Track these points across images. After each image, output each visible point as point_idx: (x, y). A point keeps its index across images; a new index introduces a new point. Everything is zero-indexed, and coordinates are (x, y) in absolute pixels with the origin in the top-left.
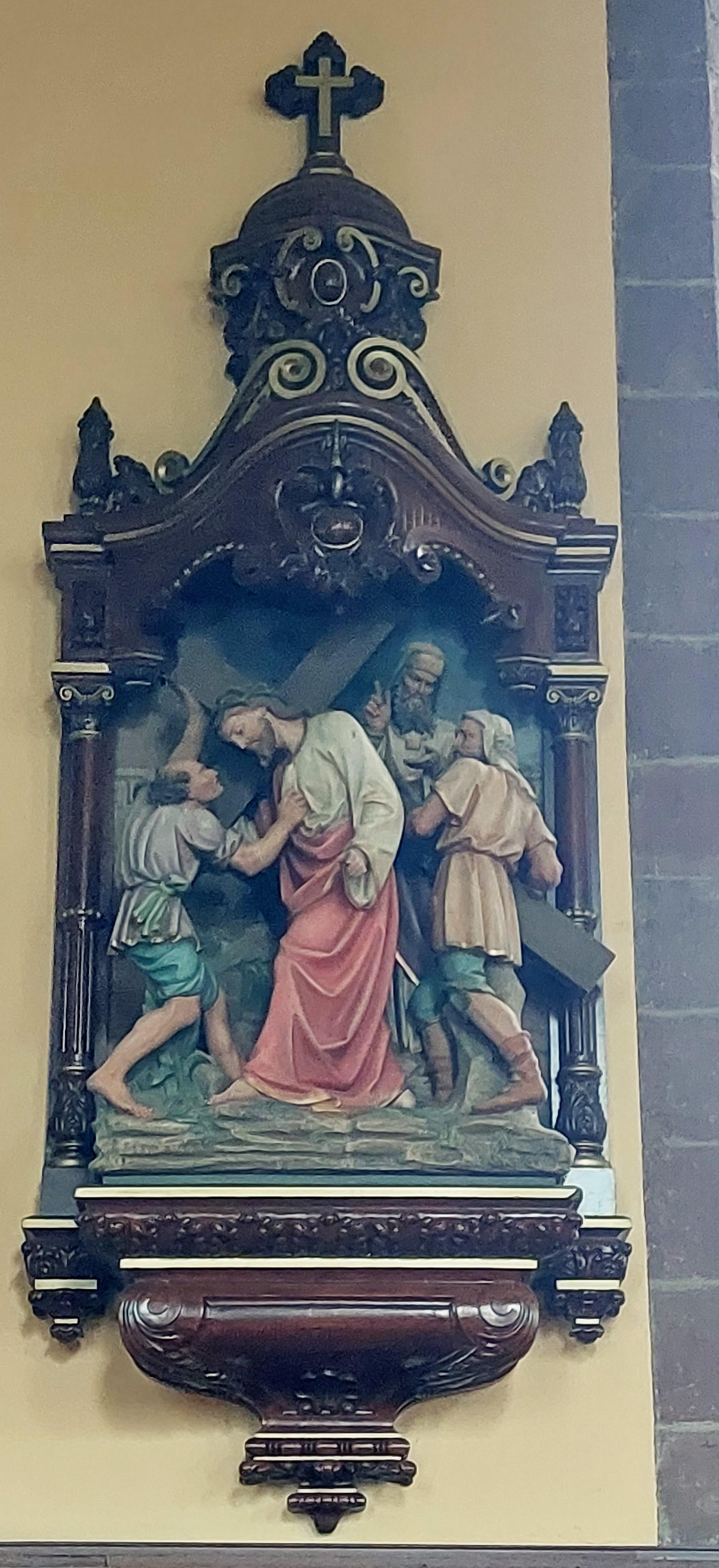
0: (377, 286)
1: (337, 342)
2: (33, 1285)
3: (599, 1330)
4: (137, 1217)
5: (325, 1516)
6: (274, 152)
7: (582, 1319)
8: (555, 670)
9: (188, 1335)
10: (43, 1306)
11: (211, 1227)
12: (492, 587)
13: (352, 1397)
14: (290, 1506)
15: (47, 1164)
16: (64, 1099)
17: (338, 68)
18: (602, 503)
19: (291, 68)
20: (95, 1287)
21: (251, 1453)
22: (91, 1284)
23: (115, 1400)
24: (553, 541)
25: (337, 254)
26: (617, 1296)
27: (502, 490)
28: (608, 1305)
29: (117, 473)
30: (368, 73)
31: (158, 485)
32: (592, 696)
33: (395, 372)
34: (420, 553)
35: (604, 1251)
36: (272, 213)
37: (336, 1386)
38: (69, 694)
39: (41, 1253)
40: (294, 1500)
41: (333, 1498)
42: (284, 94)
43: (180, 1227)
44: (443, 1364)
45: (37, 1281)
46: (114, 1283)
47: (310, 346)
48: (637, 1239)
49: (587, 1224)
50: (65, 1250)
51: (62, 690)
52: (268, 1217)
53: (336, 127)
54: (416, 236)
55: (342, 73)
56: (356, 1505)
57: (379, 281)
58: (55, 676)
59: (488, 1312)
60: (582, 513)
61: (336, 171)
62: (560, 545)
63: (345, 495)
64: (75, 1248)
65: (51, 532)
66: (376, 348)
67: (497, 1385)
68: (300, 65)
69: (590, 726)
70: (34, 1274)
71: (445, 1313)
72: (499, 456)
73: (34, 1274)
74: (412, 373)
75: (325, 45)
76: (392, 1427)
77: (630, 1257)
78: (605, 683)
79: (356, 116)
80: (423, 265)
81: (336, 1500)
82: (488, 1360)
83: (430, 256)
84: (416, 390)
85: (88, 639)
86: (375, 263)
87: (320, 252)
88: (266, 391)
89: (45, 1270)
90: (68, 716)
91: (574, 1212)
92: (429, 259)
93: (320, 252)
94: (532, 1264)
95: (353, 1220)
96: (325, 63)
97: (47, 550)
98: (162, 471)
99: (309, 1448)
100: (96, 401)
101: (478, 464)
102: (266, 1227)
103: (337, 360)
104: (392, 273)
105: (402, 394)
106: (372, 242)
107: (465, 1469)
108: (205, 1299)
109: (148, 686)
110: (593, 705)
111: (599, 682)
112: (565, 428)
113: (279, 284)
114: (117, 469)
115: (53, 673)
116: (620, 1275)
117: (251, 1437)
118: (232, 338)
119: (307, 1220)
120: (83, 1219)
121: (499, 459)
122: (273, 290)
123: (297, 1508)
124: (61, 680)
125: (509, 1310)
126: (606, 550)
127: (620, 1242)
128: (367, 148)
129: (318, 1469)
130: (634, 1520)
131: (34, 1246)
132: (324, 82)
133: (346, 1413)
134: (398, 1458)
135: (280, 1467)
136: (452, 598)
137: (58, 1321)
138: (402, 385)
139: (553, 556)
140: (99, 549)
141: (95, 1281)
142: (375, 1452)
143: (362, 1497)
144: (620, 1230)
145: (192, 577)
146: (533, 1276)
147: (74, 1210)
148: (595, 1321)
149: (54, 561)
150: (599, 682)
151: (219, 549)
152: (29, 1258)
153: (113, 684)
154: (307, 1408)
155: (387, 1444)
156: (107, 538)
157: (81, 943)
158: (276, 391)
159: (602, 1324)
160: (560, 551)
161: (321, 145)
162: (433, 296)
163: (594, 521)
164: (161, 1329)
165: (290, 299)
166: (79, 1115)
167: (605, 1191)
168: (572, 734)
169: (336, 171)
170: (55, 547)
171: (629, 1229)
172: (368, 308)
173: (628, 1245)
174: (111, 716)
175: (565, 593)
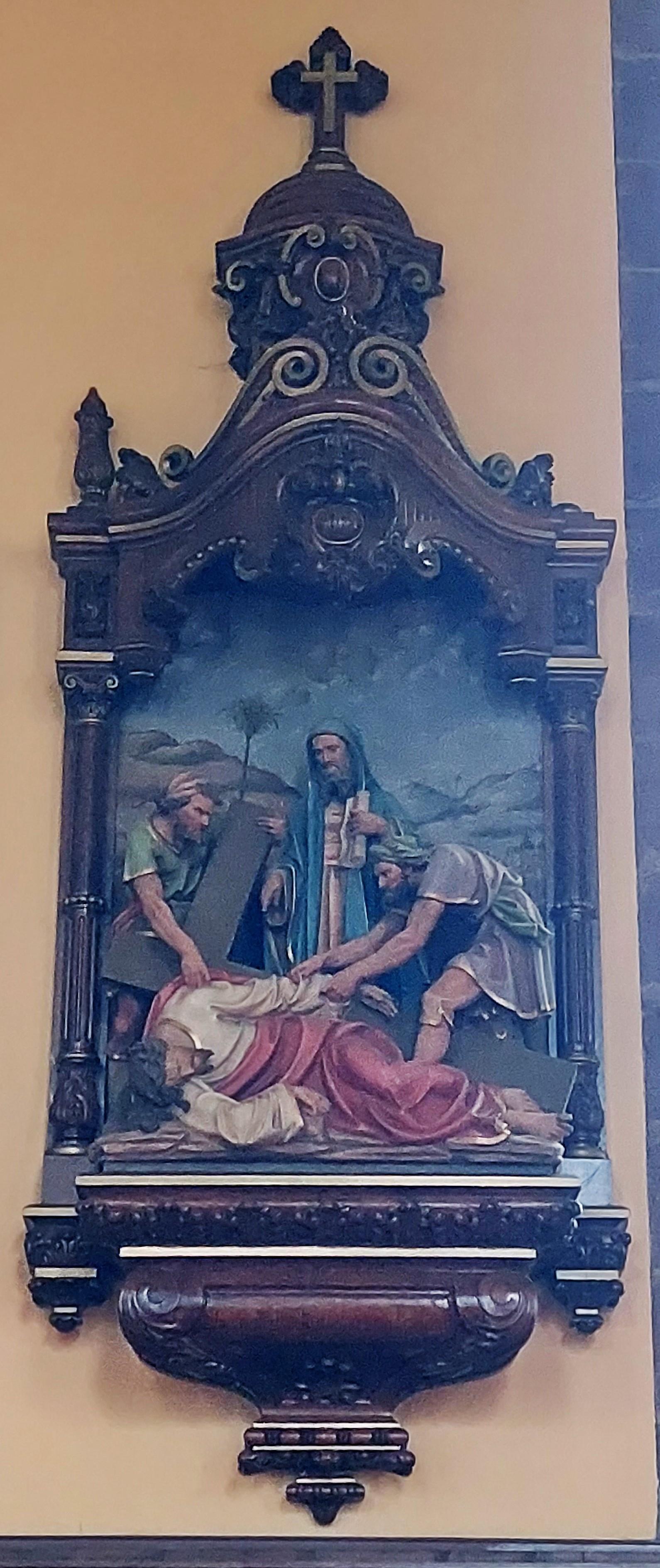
1: (340, 341)
2: (32, 1272)
3: (75, 1318)
5: (324, 1507)
6: (282, 147)
7: (584, 1310)
9: (197, 1323)
10: (43, 1293)
11: (452, 1217)
13: (351, 1387)
14: (289, 1497)
15: (47, 1153)
16: (65, 1086)
17: (343, 63)
19: (296, 63)
20: (95, 1275)
21: (249, 1443)
22: (93, 1273)
23: (109, 1385)
24: (552, 535)
25: (343, 253)
28: (608, 1295)
29: (121, 465)
30: (372, 67)
33: (397, 373)
35: (604, 1240)
36: (274, 207)
39: (41, 1241)
40: (294, 1490)
41: (313, 1489)
42: (290, 88)
43: (501, 1217)
44: (459, 1357)
45: (37, 1270)
46: (115, 1272)
47: (320, 352)
48: (639, 1229)
50: (65, 1239)
51: (67, 677)
52: (428, 1207)
53: (340, 129)
54: (417, 233)
55: (348, 68)
56: (355, 1496)
59: (487, 1302)
61: (340, 167)
63: (348, 492)
67: (492, 1378)
68: (307, 62)
71: (444, 1303)
74: (414, 371)
75: (330, 40)
76: (390, 1417)
77: (630, 1246)
78: (604, 675)
80: (424, 261)
81: (317, 1490)
87: (323, 251)
88: (270, 387)
90: (74, 701)
91: (572, 1201)
93: (323, 251)
94: (530, 1253)
95: (351, 1208)
96: (330, 59)
97: (53, 542)
98: (167, 465)
99: (307, 1436)
100: (93, 391)
105: (404, 392)
106: (375, 240)
108: (206, 1287)
111: (600, 674)
113: (282, 279)
114: (122, 461)
115: (58, 662)
117: (250, 1427)
119: (467, 1210)
120: (83, 1207)
122: (277, 283)
123: (295, 1497)
125: (508, 1299)
126: (604, 544)
128: (377, 147)
129: (317, 1459)
132: (330, 75)
136: (456, 591)
137: (58, 1310)
142: (372, 1442)
143: (363, 1487)
146: (532, 1264)
147: (75, 1199)
148: (595, 1312)
149: (58, 551)
154: (305, 1397)
156: (112, 529)
157: (83, 929)
159: (602, 1315)
160: (560, 544)
161: (328, 141)
163: (593, 514)
164: (161, 1317)
165: (293, 295)
166: (81, 1102)
169: (340, 167)
170: (60, 538)
171: (625, 1220)
173: (629, 1235)
174: (119, 702)
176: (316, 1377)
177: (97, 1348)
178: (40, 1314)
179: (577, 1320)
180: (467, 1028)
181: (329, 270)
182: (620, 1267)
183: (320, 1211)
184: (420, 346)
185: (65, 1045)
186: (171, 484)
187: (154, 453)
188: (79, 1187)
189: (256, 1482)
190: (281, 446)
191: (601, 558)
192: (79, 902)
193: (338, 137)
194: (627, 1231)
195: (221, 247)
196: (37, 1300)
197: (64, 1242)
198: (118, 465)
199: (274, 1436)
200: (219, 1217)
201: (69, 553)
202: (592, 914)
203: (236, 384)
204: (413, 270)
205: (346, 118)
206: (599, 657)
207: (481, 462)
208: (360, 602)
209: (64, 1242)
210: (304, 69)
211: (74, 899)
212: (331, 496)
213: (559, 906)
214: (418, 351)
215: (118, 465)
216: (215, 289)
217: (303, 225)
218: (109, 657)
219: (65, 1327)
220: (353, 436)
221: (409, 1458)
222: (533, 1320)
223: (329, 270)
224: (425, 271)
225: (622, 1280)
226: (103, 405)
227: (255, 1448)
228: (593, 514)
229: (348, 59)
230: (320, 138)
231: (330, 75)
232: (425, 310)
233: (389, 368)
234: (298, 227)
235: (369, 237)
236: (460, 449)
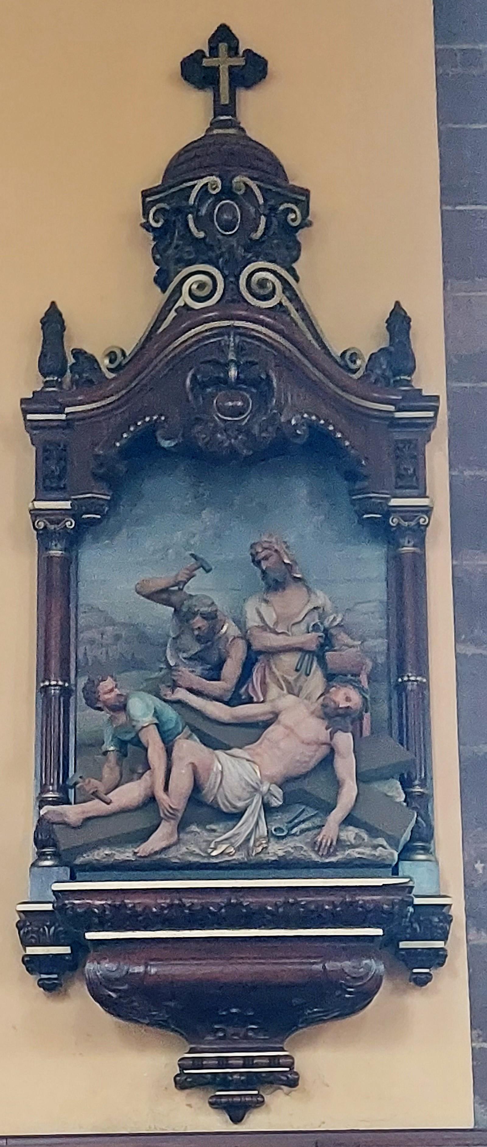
0: (263, 219)
4: (98, 903)
5: (237, 1112)
6: (189, 116)
7: (419, 968)
8: (394, 502)
10: (32, 964)
12: (347, 443)
17: (233, 50)
18: (431, 376)
20: (69, 952)
21: (182, 1067)
22: (67, 950)
24: (392, 408)
26: (441, 953)
27: (354, 371)
28: (438, 958)
31: (104, 370)
32: (422, 520)
34: (293, 422)
35: (434, 920)
36: (187, 162)
37: (243, 1020)
38: (42, 525)
39: (30, 928)
42: (195, 71)
45: (28, 948)
46: (82, 949)
48: (458, 911)
49: (417, 901)
50: (47, 926)
55: (237, 54)
56: (258, 1103)
57: (265, 215)
58: (32, 512)
60: (413, 384)
62: (399, 410)
64: (54, 924)
65: (27, 406)
66: (260, 270)
69: (421, 543)
70: (25, 944)
72: (352, 346)
73: (25, 944)
74: (287, 286)
75: (223, 35)
77: (452, 924)
79: (248, 87)
80: (297, 202)
82: (335, 1000)
83: (302, 194)
84: (290, 300)
85: (54, 485)
86: (261, 201)
87: (218, 198)
88: (180, 303)
89: (33, 941)
90: (44, 537)
92: (302, 197)
94: (379, 932)
96: (223, 47)
98: (107, 361)
99: (223, 1063)
100: (53, 303)
101: (337, 351)
102: (361, 907)
103: (232, 279)
104: (273, 209)
105: (280, 304)
106: (259, 187)
107: (338, 1077)
109: (99, 519)
110: (422, 528)
111: (428, 511)
112: (398, 322)
116: (444, 938)
118: (158, 253)
121: (353, 348)
124: (35, 514)
126: (431, 414)
127: (444, 913)
128: (259, 115)
129: (230, 1078)
130: (457, 1110)
131: (25, 922)
132: (224, 63)
133: (250, 1038)
134: (288, 1069)
135: (204, 1078)
138: (279, 297)
139: (394, 418)
140: (63, 417)
141: (69, 948)
143: (263, 1097)
144: (444, 905)
145: (129, 439)
147: (53, 898)
149: (32, 427)
150: (428, 511)
151: (147, 419)
152: (22, 932)
153: (73, 516)
155: (244, 1064)
156: (68, 410)
158: (188, 303)
160: (398, 415)
161: (225, 112)
162: (305, 224)
163: (420, 390)
167: (442, 876)
168: (408, 549)
169: (231, 131)
170: (30, 417)
171: (450, 905)
172: (257, 235)
173: (451, 916)
174: (73, 540)
175: (401, 446)
176: (229, 1020)
177: (78, 1002)
178: (32, 980)
179: (414, 976)
180: (322, 779)
181: (222, 207)
182: (445, 939)
183: (343, 903)
184: (294, 265)
185: (43, 789)
186: (110, 376)
187: (97, 349)
188: (53, 891)
189: (188, 1095)
190: (191, 346)
191: (426, 425)
192: (50, 685)
193: (230, 109)
194: (450, 913)
195: (145, 194)
196: (30, 971)
197: (46, 929)
198: (71, 360)
199: (198, 1063)
200: (154, 910)
201: (36, 428)
202: (424, 687)
203: (159, 297)
204: (288, 208)
205: (237, 93)
206: (427, 497)
207: (339, 354)
208: (249, 462)
209: (46, 929)
210: (204, 56)
211: (47, 683)
212: (224, 382)
213: (400, 680)
214: (292, 272)
215: (71, 360)
216: (143, 225)
217: (206, 176)
218: (66, 505)
219: (50, 988)
220: (243, 338)
221: (296, 1077)
222: (381, 977)
223: (222, 207)
224: (297, 210)
225: (446, 947)
226: (60, 315)
227: (186, 1072)
228: (420, 390)
229: (237, 48)
230: (219, 109)
231: (224, 63)
232: (298, 238)
233: (269, 285)
234: (202, 177)
235: (253, 185)
236: (324, 347)
